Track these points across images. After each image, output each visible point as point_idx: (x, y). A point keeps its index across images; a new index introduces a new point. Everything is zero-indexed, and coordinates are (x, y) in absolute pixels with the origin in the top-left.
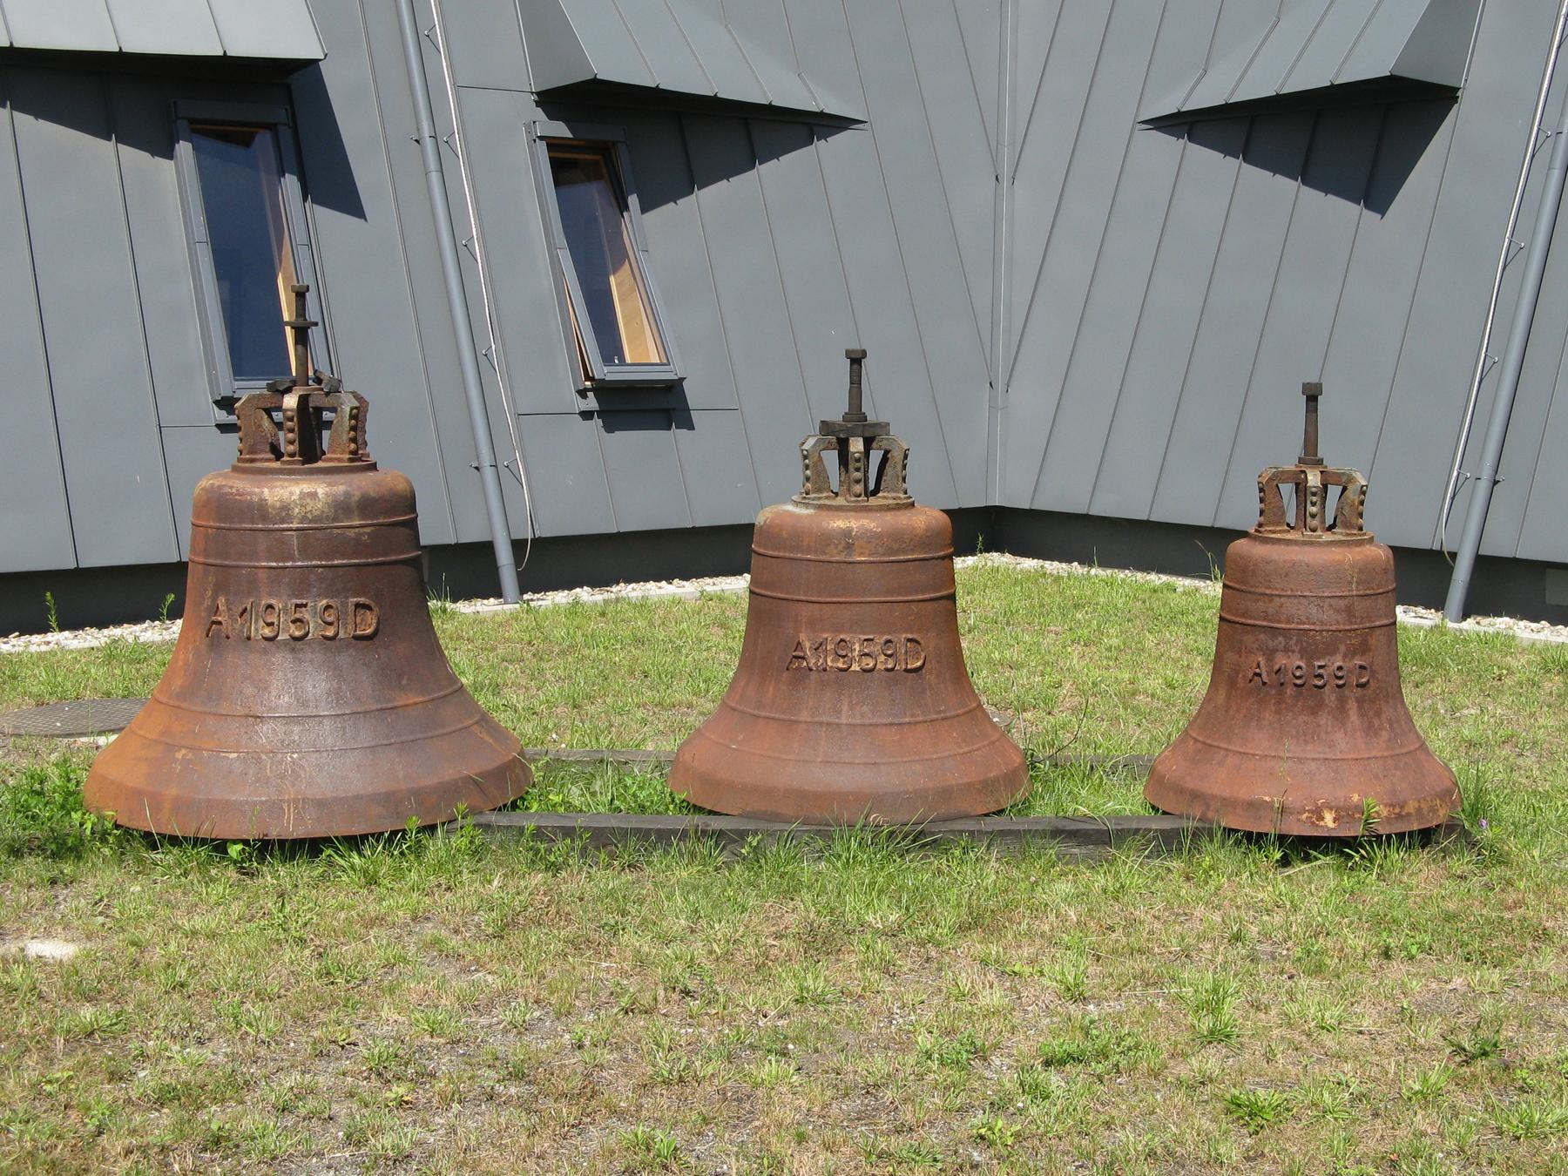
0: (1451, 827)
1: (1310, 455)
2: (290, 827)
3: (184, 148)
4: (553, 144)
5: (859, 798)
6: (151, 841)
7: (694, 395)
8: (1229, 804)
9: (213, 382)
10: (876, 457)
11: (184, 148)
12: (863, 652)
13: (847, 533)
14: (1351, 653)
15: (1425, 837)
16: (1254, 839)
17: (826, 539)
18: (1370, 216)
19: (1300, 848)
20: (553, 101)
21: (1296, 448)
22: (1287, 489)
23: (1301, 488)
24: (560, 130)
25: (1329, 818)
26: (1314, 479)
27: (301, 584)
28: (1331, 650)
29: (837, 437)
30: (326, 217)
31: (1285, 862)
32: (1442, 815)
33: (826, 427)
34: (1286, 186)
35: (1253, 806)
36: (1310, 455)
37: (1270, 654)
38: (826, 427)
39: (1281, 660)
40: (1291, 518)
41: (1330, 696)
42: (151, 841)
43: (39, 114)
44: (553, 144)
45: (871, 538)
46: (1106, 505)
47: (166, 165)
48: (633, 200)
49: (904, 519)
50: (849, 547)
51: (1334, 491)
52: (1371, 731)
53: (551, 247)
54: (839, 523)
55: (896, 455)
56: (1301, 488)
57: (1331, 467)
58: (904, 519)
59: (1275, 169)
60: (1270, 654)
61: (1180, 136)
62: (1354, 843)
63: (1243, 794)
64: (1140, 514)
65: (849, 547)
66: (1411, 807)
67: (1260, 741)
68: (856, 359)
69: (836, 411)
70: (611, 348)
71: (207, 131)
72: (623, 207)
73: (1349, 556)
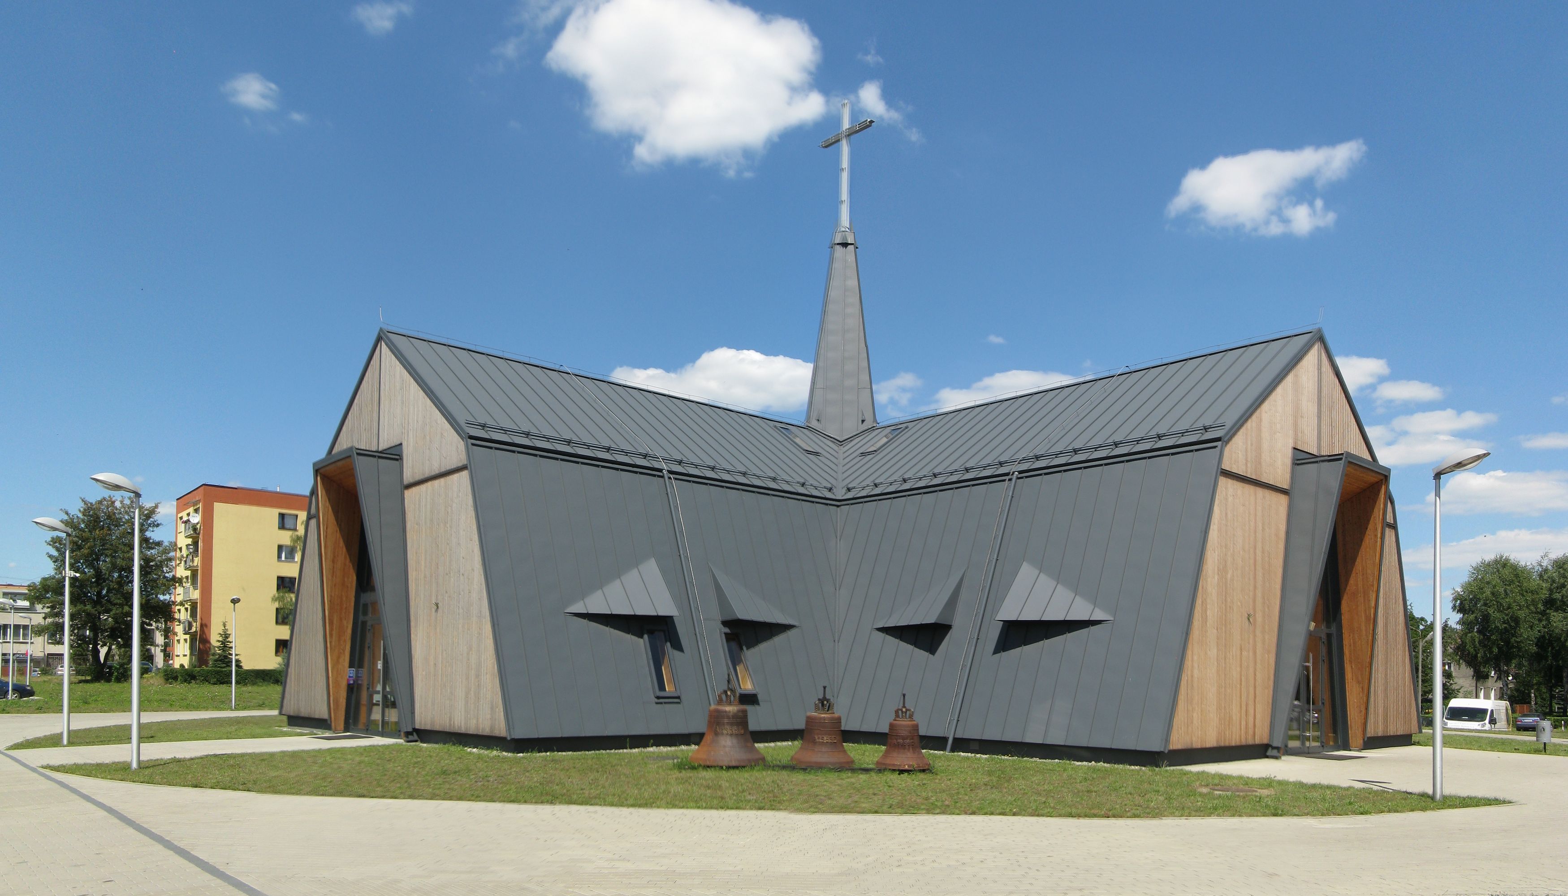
0: (928, 769)
1: (904, 706)
2: (734, 764)
3: (646, 636)
4: (726, 634)
5: (827, 763)
6: (708, 767)
7: (759, 697)
8: (890, 765)
9: (654, 692)
10: (828, 704)
11: (646, 636)
12: (826, 739)
13: (824, 717)
14: (910, 740)
15: (923, 771)
16: (894, 770)
17: (821, 718)
18: (931, 656)
19: (902, 772)
20: (725, 623)
21: (901, 705)
22: (900, 712)
23: (902, 712)
24: (727, 630)
25: (907, 767)
26: (904, 710)
27: (732, 724)
28: (907, 739)
29: (822, 701)
30: (677, 653)
31: (899, 774)
32: (927, 767)
33: (819, 700)
34: (910, 647)
35: (894, 765)
36: (904, 706)
37: (897, 739)
38: (819, 700)
39: (899, 741)
40: (901, 717)
41: (907, 747)
42: (708, 767)
43: (615, 628)
44: (726, 634)
45: (828, 718)
46: (865, 728)
47: (641, 640)
48: (744, 648)
49: (833, 715)
50: (825, 720)
51: (908, 712)
52: (914, 753)
53: (726, 660)
54: (823, 716)
55: (832, 704)
56: (902, 712)
57: (908, 708)
58: (833, 715)
59: (908, 643)
60: (897, 739)
61: (883, 633)
62: (911, 771)
63: (892, 763)
64: (873, 730)
65: (825, 720)
66: (921, 765)
67: (895, 754)
68: (825, 688)
69: (821, 697)
70: (662, 687)
71: (651, 633)
72: (742, 649)
73: (910, 723)
